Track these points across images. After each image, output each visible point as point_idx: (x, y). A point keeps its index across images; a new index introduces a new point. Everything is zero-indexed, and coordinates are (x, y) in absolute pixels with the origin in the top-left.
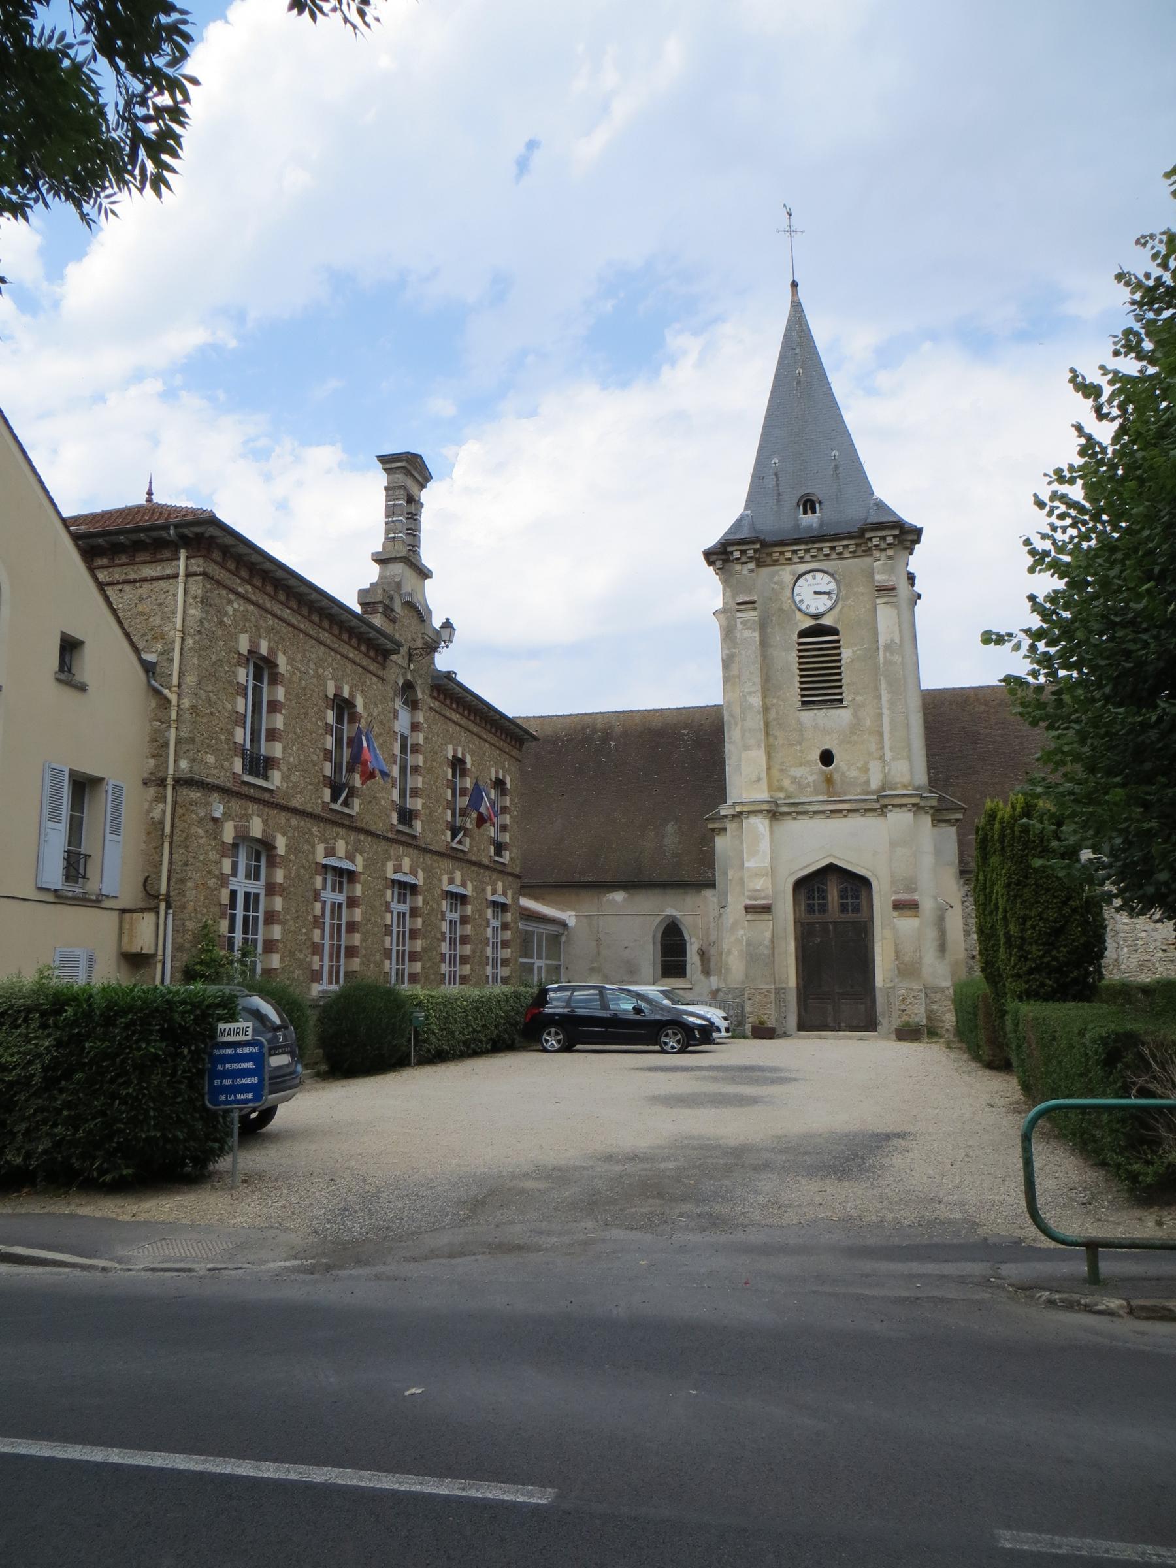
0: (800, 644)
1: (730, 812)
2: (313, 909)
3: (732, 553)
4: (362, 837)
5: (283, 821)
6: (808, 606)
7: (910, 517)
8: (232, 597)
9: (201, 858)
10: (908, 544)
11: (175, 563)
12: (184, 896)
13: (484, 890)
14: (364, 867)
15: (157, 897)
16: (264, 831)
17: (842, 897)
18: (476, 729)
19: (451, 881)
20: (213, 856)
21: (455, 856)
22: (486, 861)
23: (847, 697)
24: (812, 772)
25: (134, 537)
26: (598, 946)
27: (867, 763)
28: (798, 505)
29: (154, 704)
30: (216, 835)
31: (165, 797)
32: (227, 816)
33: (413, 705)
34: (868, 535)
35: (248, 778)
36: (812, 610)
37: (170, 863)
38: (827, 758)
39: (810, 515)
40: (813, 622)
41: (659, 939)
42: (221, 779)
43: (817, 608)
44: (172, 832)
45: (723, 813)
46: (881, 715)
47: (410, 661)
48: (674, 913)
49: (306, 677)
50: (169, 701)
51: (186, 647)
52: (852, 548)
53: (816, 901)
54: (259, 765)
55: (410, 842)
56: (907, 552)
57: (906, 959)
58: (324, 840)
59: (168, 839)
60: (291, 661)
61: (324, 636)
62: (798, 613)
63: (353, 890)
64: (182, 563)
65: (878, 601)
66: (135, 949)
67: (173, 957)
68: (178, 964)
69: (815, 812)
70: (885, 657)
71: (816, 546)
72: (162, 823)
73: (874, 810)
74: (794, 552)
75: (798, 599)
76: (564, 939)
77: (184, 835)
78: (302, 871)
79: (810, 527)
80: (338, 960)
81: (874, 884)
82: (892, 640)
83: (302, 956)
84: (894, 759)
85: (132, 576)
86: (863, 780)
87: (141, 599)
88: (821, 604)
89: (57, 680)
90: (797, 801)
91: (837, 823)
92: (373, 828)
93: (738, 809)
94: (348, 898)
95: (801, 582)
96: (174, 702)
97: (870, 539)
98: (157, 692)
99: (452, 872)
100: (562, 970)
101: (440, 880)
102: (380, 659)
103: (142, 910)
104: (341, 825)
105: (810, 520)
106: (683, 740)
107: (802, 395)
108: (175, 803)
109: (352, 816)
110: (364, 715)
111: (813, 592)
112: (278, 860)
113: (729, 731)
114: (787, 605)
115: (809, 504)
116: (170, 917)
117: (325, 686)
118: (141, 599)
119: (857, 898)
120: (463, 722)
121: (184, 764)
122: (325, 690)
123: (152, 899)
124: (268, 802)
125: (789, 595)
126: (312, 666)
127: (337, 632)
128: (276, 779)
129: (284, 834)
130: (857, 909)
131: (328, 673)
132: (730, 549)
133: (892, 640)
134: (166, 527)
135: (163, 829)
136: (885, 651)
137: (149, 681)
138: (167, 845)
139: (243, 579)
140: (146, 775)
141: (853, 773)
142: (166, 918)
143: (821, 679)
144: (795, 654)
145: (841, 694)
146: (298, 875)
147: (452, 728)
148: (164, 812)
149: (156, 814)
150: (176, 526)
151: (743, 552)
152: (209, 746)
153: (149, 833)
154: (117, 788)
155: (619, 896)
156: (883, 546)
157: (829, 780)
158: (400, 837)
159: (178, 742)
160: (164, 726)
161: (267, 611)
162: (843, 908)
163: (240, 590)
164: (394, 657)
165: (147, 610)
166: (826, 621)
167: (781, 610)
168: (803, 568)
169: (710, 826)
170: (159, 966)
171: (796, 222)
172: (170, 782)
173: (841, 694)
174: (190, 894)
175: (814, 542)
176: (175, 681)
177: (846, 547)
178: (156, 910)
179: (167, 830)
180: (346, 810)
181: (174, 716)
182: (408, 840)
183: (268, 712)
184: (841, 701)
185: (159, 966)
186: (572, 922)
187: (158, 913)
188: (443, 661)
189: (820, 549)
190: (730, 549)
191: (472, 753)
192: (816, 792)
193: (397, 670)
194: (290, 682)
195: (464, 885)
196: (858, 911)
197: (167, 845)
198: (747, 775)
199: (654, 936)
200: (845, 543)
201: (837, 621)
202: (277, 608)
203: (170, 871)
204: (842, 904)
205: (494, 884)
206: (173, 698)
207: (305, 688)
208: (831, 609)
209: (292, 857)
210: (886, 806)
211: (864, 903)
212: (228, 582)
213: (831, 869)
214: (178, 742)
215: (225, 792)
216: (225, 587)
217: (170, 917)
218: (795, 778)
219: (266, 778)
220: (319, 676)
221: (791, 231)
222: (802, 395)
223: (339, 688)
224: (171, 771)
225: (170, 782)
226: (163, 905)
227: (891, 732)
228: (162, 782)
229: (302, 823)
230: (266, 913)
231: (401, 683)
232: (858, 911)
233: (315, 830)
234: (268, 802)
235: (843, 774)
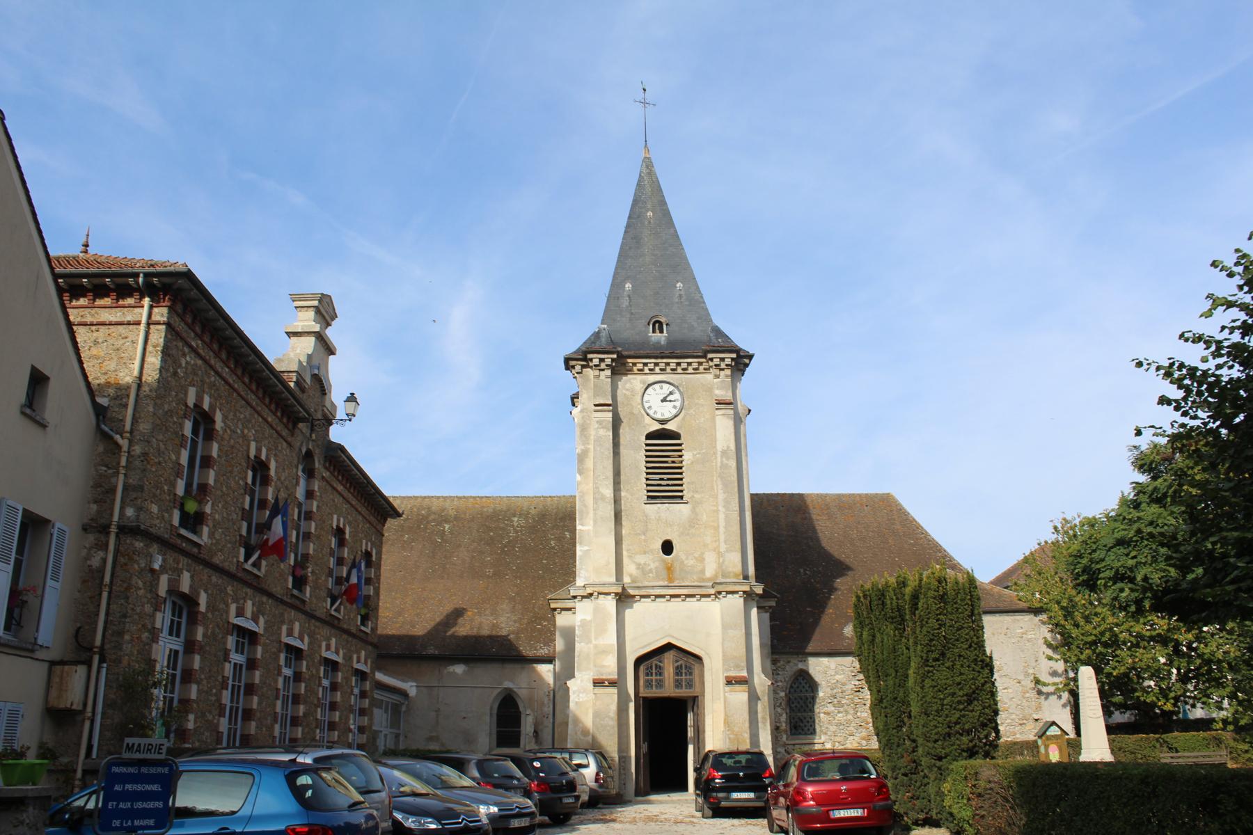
2: (223, 669)
3: (591, 360)
4: (264, 599)
5: (205, 577)
8: (186, 350)
9: (138, 610)
12: (121, 649)
13: (351, 658)
14: (265, 629)
15: (90, 649)
16: (191, 586)
17: (677, 674)
19: (328, 648)
20: (148, 608)
22: (353, 630)
23: (687, 494)
29: (101, 449)
30: (153, 587)
31: (107, 545)
32: (163, 568)
34: (710, 356)
35: (183, 532)
36: (659, 416)
37: (107, 614)
38: (667, 547)
41: (495, 711)
42: (159, 528)
44: (112, 582)
45: (573, 593)
46: (717, 511)
48: (511, 685)
50: (119, 447)
52: (695, 365)
53: (654, 677)
54: (193, 521)
55: (299, 606)
57: (736, 729)
58: (236, 600)
60: (225, 418)
61: (252, 397)
63: (255, 652)
64: (145, 310)
65: (718, 412)
67: (103, 713)
69: (657, 596)
74: (645, 364)
75: (646, 405)
76: (404, 708)
78: (217, 630)
79: (659, 343)
80: (236, 724)
81: (706, 661)
83: (210, 717)
85: (89, 319)
88: (667, 411)
89: (23, 413)
93: (589, 590)
94: (248, 660)
95: (650, 390)
96: (125, 448)
98: (106, 437)
100: (401, 738)
101: (320, 646)
102: (290, 426)
104: (250, 585)
107: (650, 233)
108: (117, 551)
109: (258, 577)
110: (275, 478)
112: (200, 617)
114: (637, 409)
116: (104, 671)
117: (248, 447)
118: (96, 342)
119: (691, 674)
120: (346, 493)
121: (130, 512)
123: (81, 650)
124: (199, 558)
128: (204, 537)
129: (206, 591)
130: (690, 685)
131: (251, 434)
132: (590, 356)
134: (136, 275)
135: (103, 578)
137: (98, 425)
140: (86, 521)
142: (99, 672)
146: (213, 633)
147: (338, 499)
148: (104, 561)
149: (95, 562)
150: (146, 275)
152: (155, 496)
153: (84, 582)
154: (61, 531)
155: (459, 669)
156: (723, 365)
157: (669, 569)
159: (125, 488)
160: (110, 471)
161: (211, 367)
162: (678, 684)
163: (193, 344)
164: (300, 425)
165: (102, 354)
167: (632, 413)
168: (652, 378)
169: (553, 606)
171: (649, 96)
172: (113, 529)
174: (127, 648)
175: (662, 358)
176: (128, 427)
177: (689, 364)
179: (107, 579)
180: (255, 571)
181: (123, 462)
182: (298, 603)
183: (201, 467)
184: (681, 497)
186: (412, 692)
188: (336, 434)
189: (667, 364)
190: (590, 356)
194: (223, 439)
195: (337, 652)
198: (593, 559)
199: (491, 709)
201: (680, 427)
203: (106, 622)
204: (677, 681)
206: (124, 443)
207: (233, 447)
209: (210, 615)
210: (720, 593)
212: (184, 335)
213: (669, 647)
214: (126, 488)
215: (165, 545)
217: (104, 671)
219: (195, 532)
220: (244, 436)
222: (650, 233)
223: (259, 450)
224: (116, 518)
225: (113, 529)
226: (96, 658)
228: (104, 530)
229: (220, 581)
231: (304, 450)
233: (229, 589)
234: (199, 558)
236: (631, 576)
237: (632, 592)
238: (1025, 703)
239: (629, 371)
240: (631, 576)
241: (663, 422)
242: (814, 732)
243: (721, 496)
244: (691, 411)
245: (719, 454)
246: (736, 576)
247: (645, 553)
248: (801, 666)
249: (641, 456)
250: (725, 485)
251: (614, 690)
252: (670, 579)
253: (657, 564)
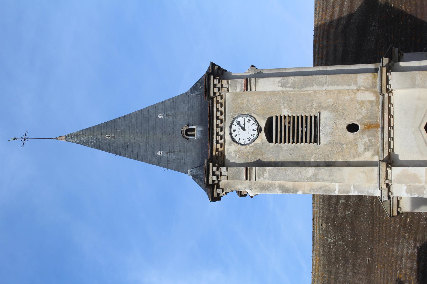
0: (276, 142)
1: (386, 192)
3: (213, 181)
6: (253, 135)
10: (220, 72)
24: (361, 138)
27: (358, 102)
28: (188, 139)
36: (255, 133)
38: (353, 128)
39: (195, 132)
43: (254, 130)
45: (386, 199)
46: (326, 91)
56: (225, 72)
62: (256, 141)
69: (389, 136)
70: (290, 87)
71: (215, 128)
73: (390, 98)
75: (247, 142)
79: (201, 132)
82: (279, 82)
84: (356, 84)
86: (369, 104)
90: (380, 148)
91: (395, 122)
93: (384, 186)
95: (236, 139)
106: (335, 242)
111: (241, 137)
113: (331, 191)
114: (250, 148)
115: (189, 132)
125: (244, 147)
133: (279, 82)
136: (286, 87)
141: (364, 111)
144: (282, 145)
145: (311, 117)
156: (219, 85)
157: (369, 127)
166: (263, 124)
167: (253, 153)
168: (228, 137)
169: (395, 214)
171: (20, 135)
173: (311, 117)
175: (213, 129)
190: (210, 182)
192: (375, 136)
198: (361, 183)
200: (215, 110)
201: (264, 117)
208: (256, 121)
218: (365, 148)
221: (25, 139)
227: (338, 85)
235: (364, 117)
236: (373, 155)
237: (386, 155)
239: (222, 154)
240: (373, 155)
241: (260, 130)
244: (252, 109)
245: (284, 89)
247: (356, 145)
250: (307, 85)
252: (377, 126)
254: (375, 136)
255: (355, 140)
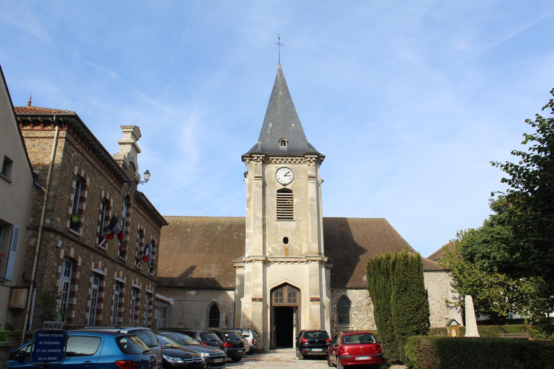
2: (88, 291)
3: (254, 157)
4: (107, 260)
6: (281, 181)
7: (321, 152)
8: (74, 150)
11: (52, 132)
12: (43, 282)
14: (107, 274)
17: (289, 296)
18: (148, 218)
21: (137, 271)
22: (146, 275)
25: (34, 118)
26: (183, 313)
27: (301, 243)
29: (35, 193)
30: (57, 254)
31: (37, 236)
32: (62, 246)
33: (128, 205)
34: (306, 156)
36: (283, 183)
37: (37, 266)
38: (286, 240)
40: (284, 187)
41: (209, 311)
42: (61, 229)
44: (39, 252)
45: (244, 260)
46: (308, 225)
47: (129, 186)
49: (95, 188)
50: (44, 192)
51: (54, 169)
52: (299, 160)
54: (76, 226)
55: (122, 264)
58: (94, 261)
59: (37, 255)
60: (91, 180)
66: (17, 306)
67: (35, 310)
68: (37, 314)
69: (281, 262)
72: (35, 247)
74: (277, 160)
75: (278, 178)
76: (168, 310)
77: (45, 254)
79: (283, 150)
80: (93, 315)
83: (82, 312)
85: (31, 135)
87: (34, 146)
88: (286, 180)
92: (111, 257)
93: (251, 259)
96: (46, 193)
97: (307, 158)
98: (38, 188)
99: (135, 279)
101: (131, 282)
102: (120, 184)
103: (23, 288)
104: (101, 254)
105: (284, 148)
107: (281, 102)
108: (42, 238)
110: (113, 207)
114: (274, 179)
115: (283, 142)
116: (35, 291)
119: (295, 296)
120: (144, 214)
121: (48, 221)
122: (101, 195)
123: (25, 282)
124: (78, 242)
126: (97, 184)
127: (107, 170)
129: (81, 257)
130: (295, 301)
131: (102, 188)
134: (52, 116)
137: (34, 182)
138: (36, 258)
139: (79, 143)
140: (28, 225)
142: (33, 292)
143: (285, 211)
147: (141, 217)
148: (36, 243)
149: (32, 243)
150: (57, 116)
151: (258, 157)
152: (59, 214)
153: (27, 252)
154: (17, 229)
155: (193, 293)
157: (286, 250)
158: (120, 262)
159: (46, 211)
160: (40, 203)
162: (289, 301)
164: (124, 184)
165: (36, 151)
166: (288, 187)
167: (271, 181)
170: (27, 315)
172: (40, 229)
174: (45, 281)
175: (285, 157)
176: (48, 183)
178: (28, 288)
179: (37, 251)
180: (103, 248)
181: (45, 199)
184: (292, 218)
185: (27, 315)
187: (29, 289)
189: (287, 160)
190: (253, 155)
191: (146, 228)
192: (281, 254)
193: (125, 189)
194: (90, 190)
195: (139, 285)
196: (282, 301)
197: (36, 258)
198: (253, 245)
201: (292, 188)
202: (88, 157)
203: (36, 270)
204: (289, 299)
205: (148, 285)
206: (46, 191)
209: (83, 267)
210: (308, 261)
211: (298, 299)
212: (73, 143)
213: (285, 284)
215: (63, 235)
216: (72, 145)
217: (35, 291)
219: (77, 230)
220: (99, 188)
222: (281, 102)
223: (106, 194)
224: (41, 224)
225: (40, 229)
226: (32, 286)
228: (36, 229)
230: (70, 292)
231: (126, 195)
232: (282, 301)
234: (78, 242)
236: (269, 253)
237: (270, 260)
238: (442, 311)
241: (285, 185)
242: (349, 323)
243: (310, 218)
244: (297, 181)
246: (316, 253)
248: (343, 293)
249: (275, 200)
251: (261, 303)
252: (287, 254)
253: (281, 248)
254: (281, 254)
255: (279, 242)
